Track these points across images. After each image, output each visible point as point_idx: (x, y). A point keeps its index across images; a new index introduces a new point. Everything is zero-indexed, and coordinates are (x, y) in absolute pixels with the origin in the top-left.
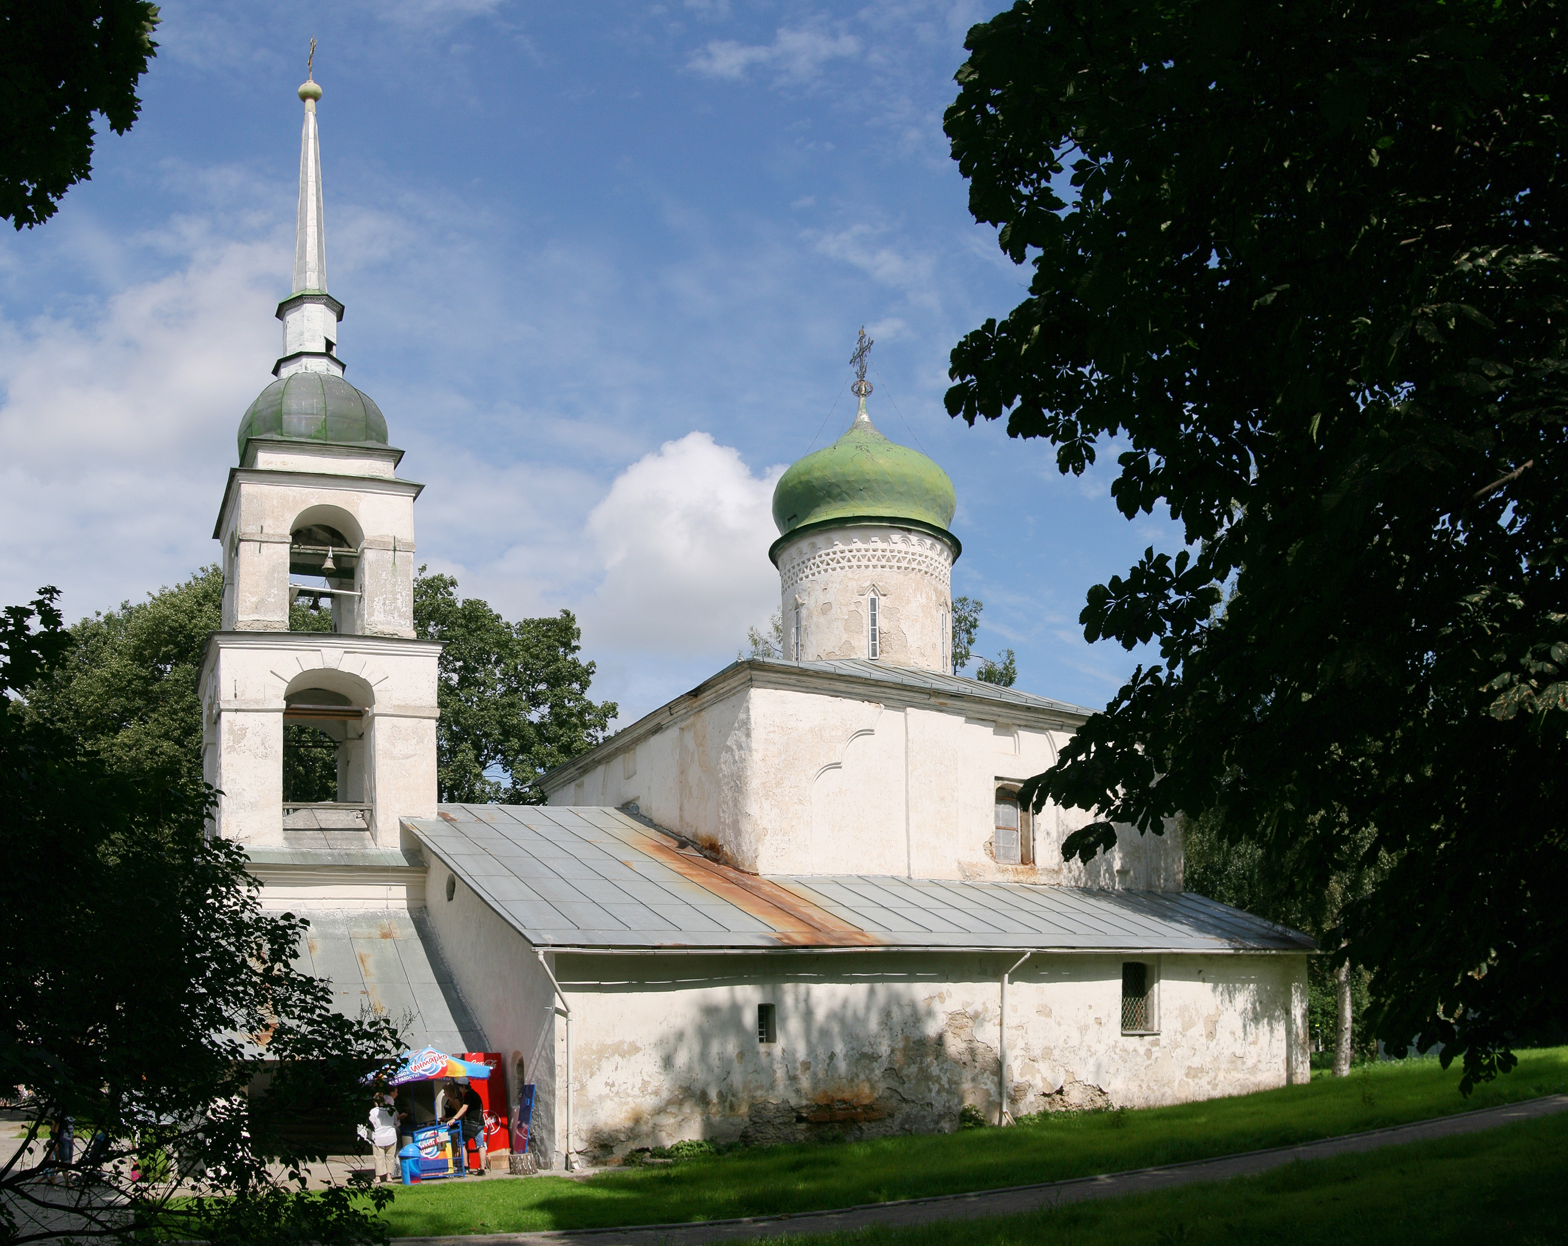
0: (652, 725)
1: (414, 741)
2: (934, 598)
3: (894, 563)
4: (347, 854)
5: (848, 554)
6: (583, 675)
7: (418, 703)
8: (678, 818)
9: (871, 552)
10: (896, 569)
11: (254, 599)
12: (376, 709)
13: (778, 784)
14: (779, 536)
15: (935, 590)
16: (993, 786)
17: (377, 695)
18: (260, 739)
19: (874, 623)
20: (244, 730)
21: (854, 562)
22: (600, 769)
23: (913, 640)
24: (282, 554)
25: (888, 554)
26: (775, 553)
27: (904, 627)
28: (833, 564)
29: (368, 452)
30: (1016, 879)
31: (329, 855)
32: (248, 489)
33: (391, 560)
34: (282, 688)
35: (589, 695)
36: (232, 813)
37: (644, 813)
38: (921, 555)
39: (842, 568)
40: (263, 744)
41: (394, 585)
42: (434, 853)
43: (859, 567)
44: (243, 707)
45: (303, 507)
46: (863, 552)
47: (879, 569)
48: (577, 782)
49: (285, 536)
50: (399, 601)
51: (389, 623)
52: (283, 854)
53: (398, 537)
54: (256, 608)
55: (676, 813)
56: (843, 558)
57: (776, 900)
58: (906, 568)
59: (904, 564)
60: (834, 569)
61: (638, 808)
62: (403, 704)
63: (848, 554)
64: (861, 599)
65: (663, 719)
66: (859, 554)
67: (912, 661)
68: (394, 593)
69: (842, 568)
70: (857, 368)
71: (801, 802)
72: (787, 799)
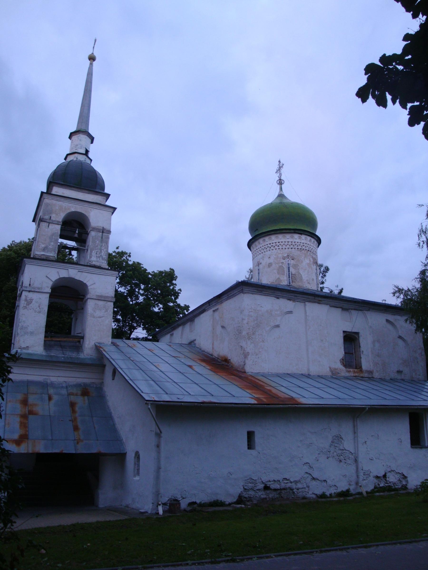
0: (201, 309)
1: (104, 311)
2: (312, 260)
3: (296, 247)
4: (70, 357)
5: (278, 244)
6: (177, 295)
7: (106, 295)
8: (212, 349)
9: (287, 243)
10: (296, 249)
11: (43, 246)
12: (88, 296)
13: (253, 334)
14: (251, 238)
15: (312, 257)
16: (342, 335)
17: (90, 290)
18: (38, 304)
19: (289, 271)
20: (31, 300)
21: (280, 247)
22: (180, 328)
23: (305, 276)
24: (57, 228)
25: (293, 243)
26: (250, 244)
27: (301, 272)
28: (272, 248)
29: (97, 193)
30: (354, 375)
31: (63, 357)
32: (47, 200)
33: (101, 236)
34: (50, 284)
35: (179, 301)
36: (22, 336)
37: (198, 347)
38: (306, 244)
39: (276, 249)
40: (39, 307)
41: (101, 246)
42: (107, 358)
43: (282, 248)
44: (32, 290)
45: (68, 211)
46: (284, 243)
47: (290, 249)
48: (171, 333)
49: (59, 222)
50: (103, 253)
51: (98, 261)
52: (42, 355)
53: (105, 227)
54: (44, 249)
55: (211, 346)
56: (276, 245)
57: (251, 383)
58: (301, 249)
59: (300, 247)
60: (273, 250)
61: (195, 344)
62: (100, 295)
63: (278, 244)
64: (283, 261)
65: (206, 307)
66: (282, 244)
67: (305, 286)
68: (101, 250)
69: (276, 249)
70: (278, 174)
71: (263, 341)
72: (257, 340)
